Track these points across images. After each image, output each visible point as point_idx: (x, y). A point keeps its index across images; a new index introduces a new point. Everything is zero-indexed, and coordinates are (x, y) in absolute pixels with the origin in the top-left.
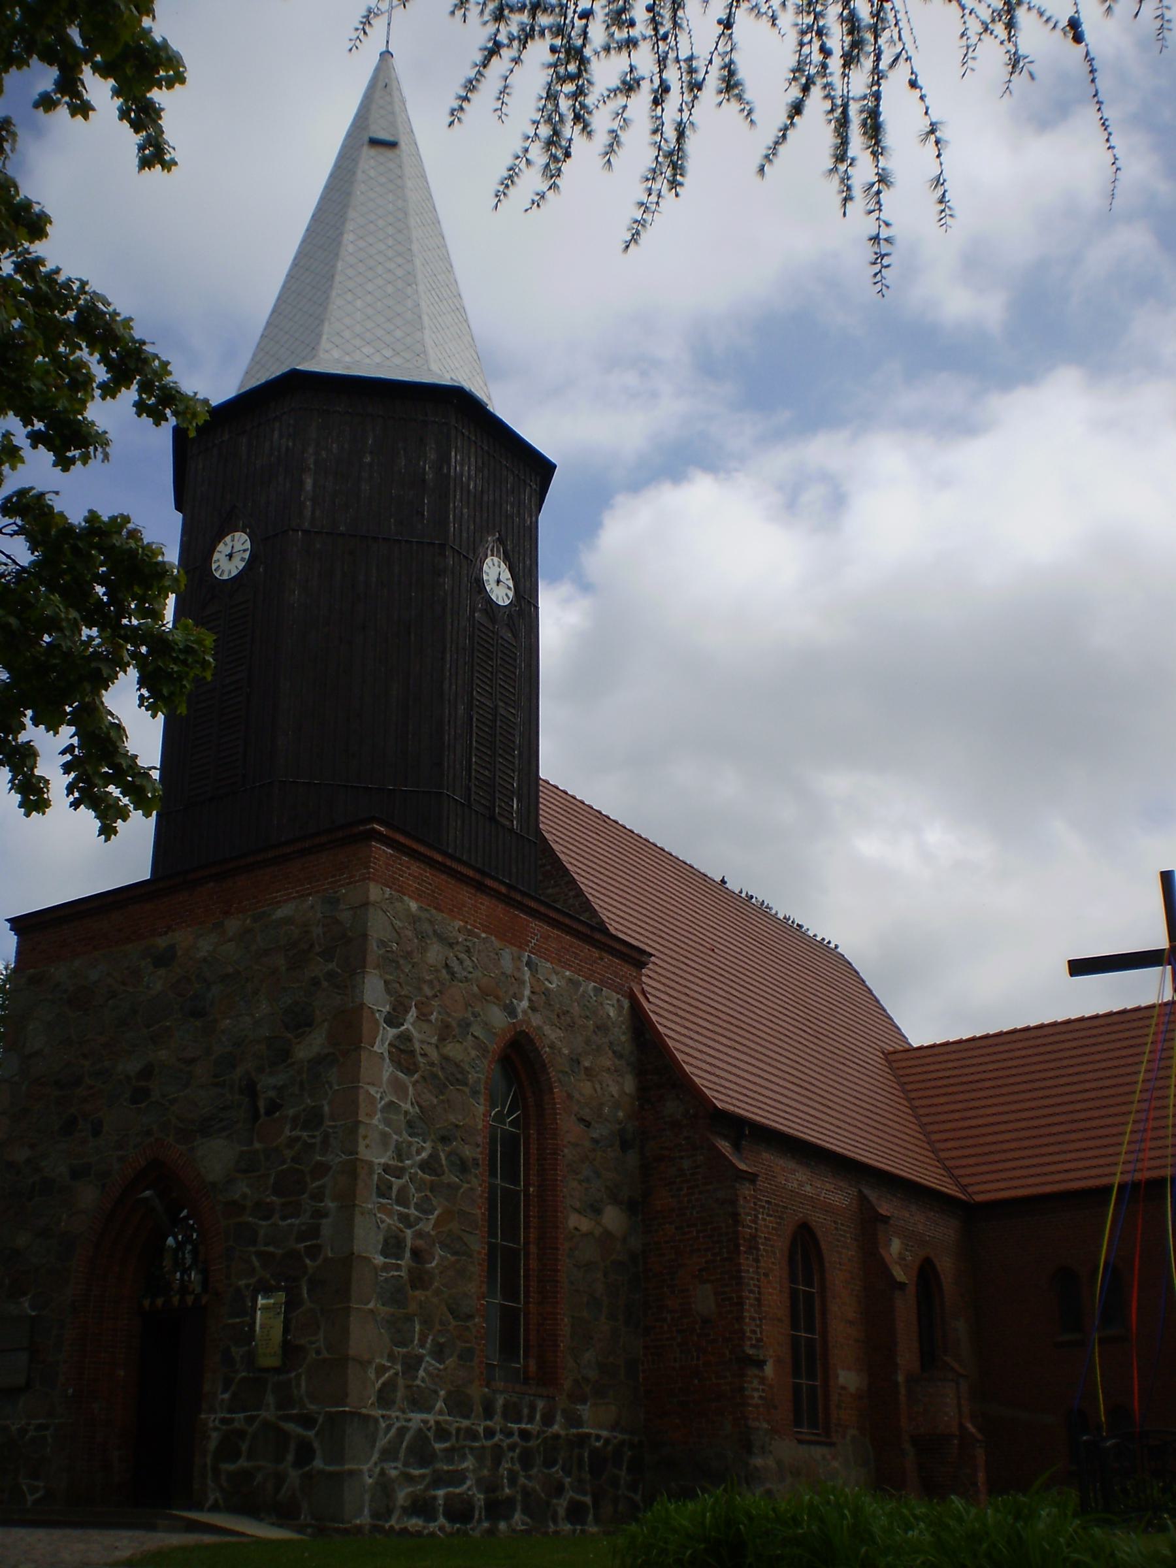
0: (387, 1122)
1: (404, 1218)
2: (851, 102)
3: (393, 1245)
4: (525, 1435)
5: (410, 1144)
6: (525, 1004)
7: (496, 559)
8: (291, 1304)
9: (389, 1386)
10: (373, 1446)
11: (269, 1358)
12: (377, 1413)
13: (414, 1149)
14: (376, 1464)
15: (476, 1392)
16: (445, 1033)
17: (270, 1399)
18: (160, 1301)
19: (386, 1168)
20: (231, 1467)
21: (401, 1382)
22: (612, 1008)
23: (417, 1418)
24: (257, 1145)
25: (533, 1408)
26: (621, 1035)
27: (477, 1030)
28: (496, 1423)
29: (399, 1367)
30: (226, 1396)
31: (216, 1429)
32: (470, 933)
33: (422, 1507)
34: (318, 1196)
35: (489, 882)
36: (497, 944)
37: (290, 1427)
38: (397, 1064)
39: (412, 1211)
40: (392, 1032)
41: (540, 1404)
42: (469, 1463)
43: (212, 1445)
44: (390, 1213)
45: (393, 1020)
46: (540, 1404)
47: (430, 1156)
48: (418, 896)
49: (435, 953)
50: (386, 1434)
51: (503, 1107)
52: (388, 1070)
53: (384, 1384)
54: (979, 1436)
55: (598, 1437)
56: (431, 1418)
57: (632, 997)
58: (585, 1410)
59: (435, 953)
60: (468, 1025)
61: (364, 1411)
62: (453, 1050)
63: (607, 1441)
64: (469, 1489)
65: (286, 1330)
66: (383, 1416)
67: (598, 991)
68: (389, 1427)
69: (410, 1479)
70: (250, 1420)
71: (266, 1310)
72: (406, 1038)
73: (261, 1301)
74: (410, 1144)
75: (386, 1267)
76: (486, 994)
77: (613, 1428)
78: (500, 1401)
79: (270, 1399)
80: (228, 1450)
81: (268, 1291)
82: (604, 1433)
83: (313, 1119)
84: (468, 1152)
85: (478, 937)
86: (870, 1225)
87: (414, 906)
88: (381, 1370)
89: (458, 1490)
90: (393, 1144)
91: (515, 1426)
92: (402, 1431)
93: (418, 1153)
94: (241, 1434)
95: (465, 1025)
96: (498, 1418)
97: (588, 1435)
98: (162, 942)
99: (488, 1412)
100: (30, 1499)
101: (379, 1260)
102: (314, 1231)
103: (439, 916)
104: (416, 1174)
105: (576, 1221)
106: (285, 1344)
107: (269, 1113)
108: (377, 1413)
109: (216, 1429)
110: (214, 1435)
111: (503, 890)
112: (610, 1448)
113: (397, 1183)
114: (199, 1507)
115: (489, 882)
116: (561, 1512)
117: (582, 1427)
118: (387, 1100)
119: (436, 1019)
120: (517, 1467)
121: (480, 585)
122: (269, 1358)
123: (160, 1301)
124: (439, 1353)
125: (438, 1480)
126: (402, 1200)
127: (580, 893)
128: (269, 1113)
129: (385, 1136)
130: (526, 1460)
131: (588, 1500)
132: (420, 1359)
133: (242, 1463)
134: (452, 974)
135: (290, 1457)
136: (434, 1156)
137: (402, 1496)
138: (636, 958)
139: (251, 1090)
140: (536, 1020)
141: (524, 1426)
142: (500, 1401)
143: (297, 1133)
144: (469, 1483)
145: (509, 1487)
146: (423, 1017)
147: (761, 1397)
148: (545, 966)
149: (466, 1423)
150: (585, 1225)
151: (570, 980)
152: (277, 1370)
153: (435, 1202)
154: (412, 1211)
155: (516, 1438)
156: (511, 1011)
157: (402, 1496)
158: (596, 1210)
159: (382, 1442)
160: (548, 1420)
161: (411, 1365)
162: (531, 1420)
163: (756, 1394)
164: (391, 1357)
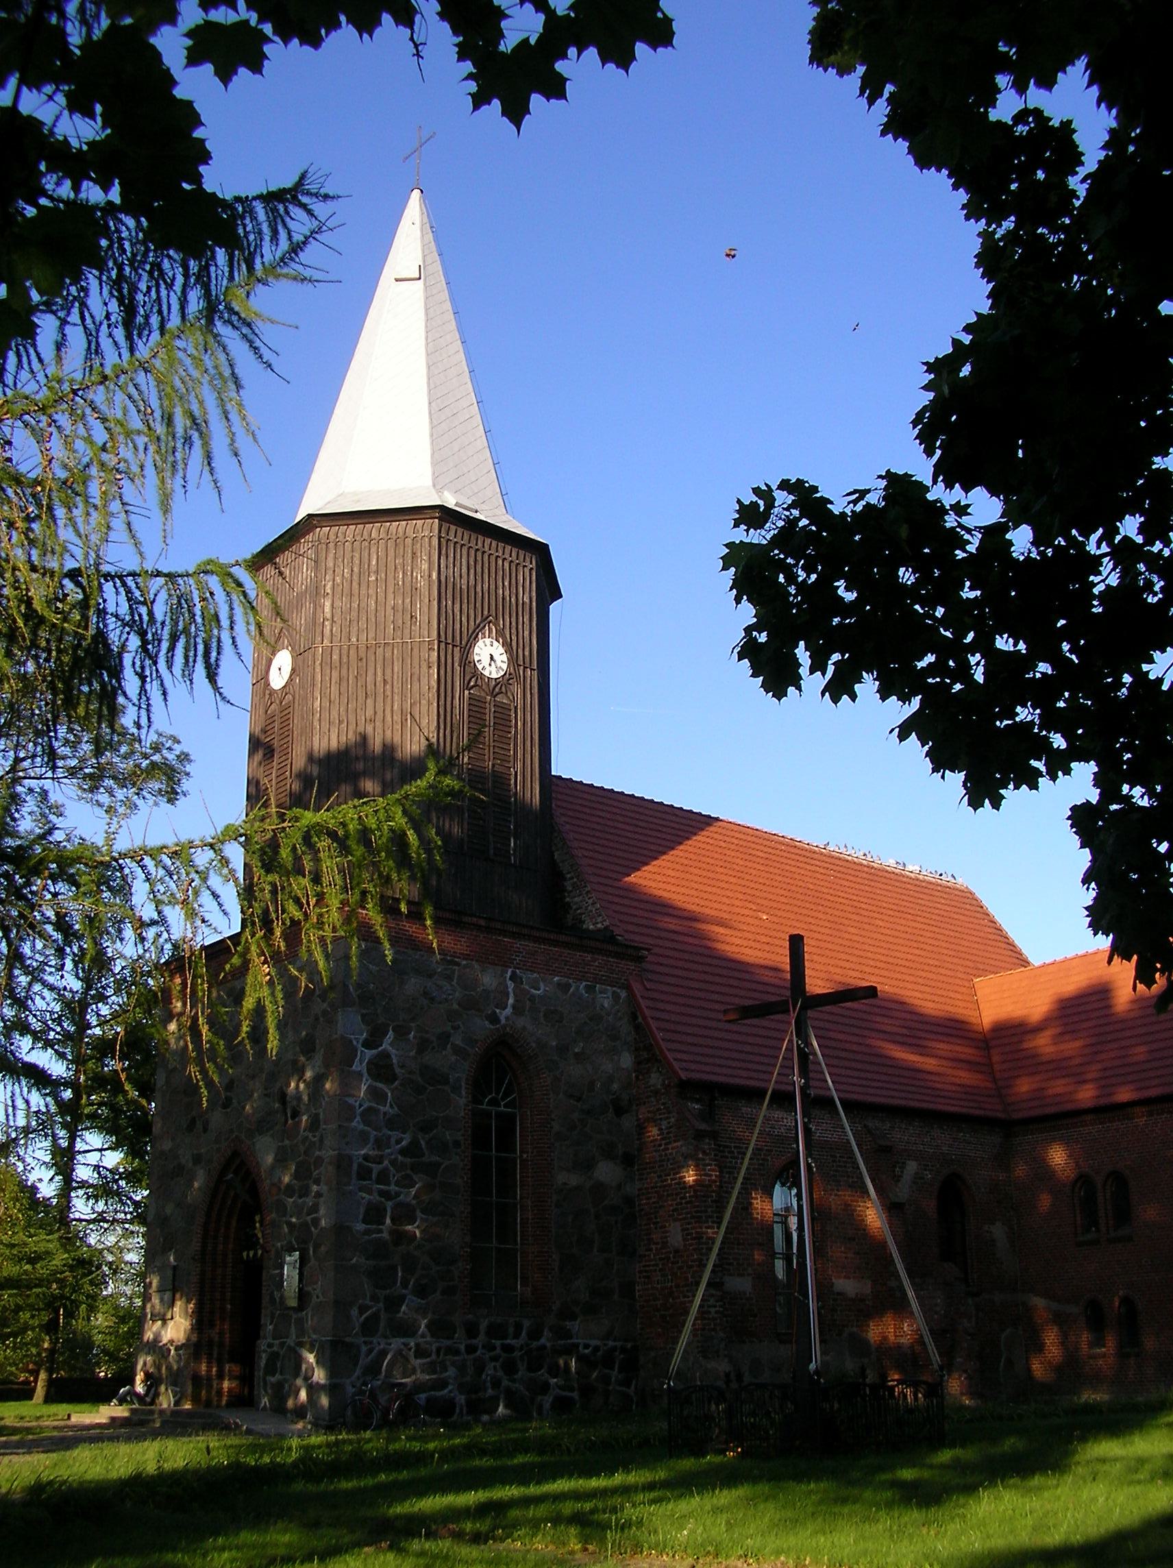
1: (386, 1195)
5: (390, 1137)
6: (509, 1011)
7: (488, 641)
10: (356, 1364)
13: (393, 1140)
14: (358, 1378)
19: (366, 1158)
21: (383, 1315)
24: (287, 1142)
25: (519, 1327)
27: (457, 1040)
29: (381, 1305)
31: (265, 1351)
35: (466, 919)
40: (370, 1053)
41: (527, 1323)
42: (451, 1372)
44: (370, 1192)
45: (368, 1044)
46: (527, 1323)
47: (411, 1143)
50: (367, 1356)
51: (497, 1093)
53: (367, 1319)
55: (586, 1346)
60: (448, 1036)
61: (348, 1339)
63: (596, 1349)
64: (450, 1392)
65: (300, 1280)
66: (365, 1343)
67: (589, 989)
68: (370, 1351)
70: (282, 1345)
72: (386, 1055)
74: (390, 1137)
75: (367, 1232)
78: (483, 1326)
85: (458, 964)
88: (362, 1309)
90: (372, 1140)
91: (498, 1343)
93: (398, 1142)
95: (444, 1038)
97: (577, 1346)
98: (428, 911)
101: (360, 1227)
104: (396, 1159)
106: (300, 1290)
109: (265, 1351)
110: (264, 1355)
111: (482, 922)
112: (600, 1353)
113: (376, 1168)
115: (466, 919)
116: (547, 1406)
117: (571, 1338)
118: (365, 1106)
119: (415, 1037)
120: (500, 1373)
126: (383, 1178)
129: (363, 1133)
131: (575, 1395)
136: (414, 1143)
140: (521, 1022)
141: (508, 1341)
142: (483, 1326)
144: (450, 1387)
145: (493, 1389)
146: (401, 1033)
147: (716, 1312)
150: (574, 1180)
151: (559, 984)
153: (415, 1178)
155: (498, 1351)
156: (494, 1019)
158: (587, 1166)
159: (364, 1361)
160: (535, 1334)
162: (516, 1336)
163: (713, 1310)
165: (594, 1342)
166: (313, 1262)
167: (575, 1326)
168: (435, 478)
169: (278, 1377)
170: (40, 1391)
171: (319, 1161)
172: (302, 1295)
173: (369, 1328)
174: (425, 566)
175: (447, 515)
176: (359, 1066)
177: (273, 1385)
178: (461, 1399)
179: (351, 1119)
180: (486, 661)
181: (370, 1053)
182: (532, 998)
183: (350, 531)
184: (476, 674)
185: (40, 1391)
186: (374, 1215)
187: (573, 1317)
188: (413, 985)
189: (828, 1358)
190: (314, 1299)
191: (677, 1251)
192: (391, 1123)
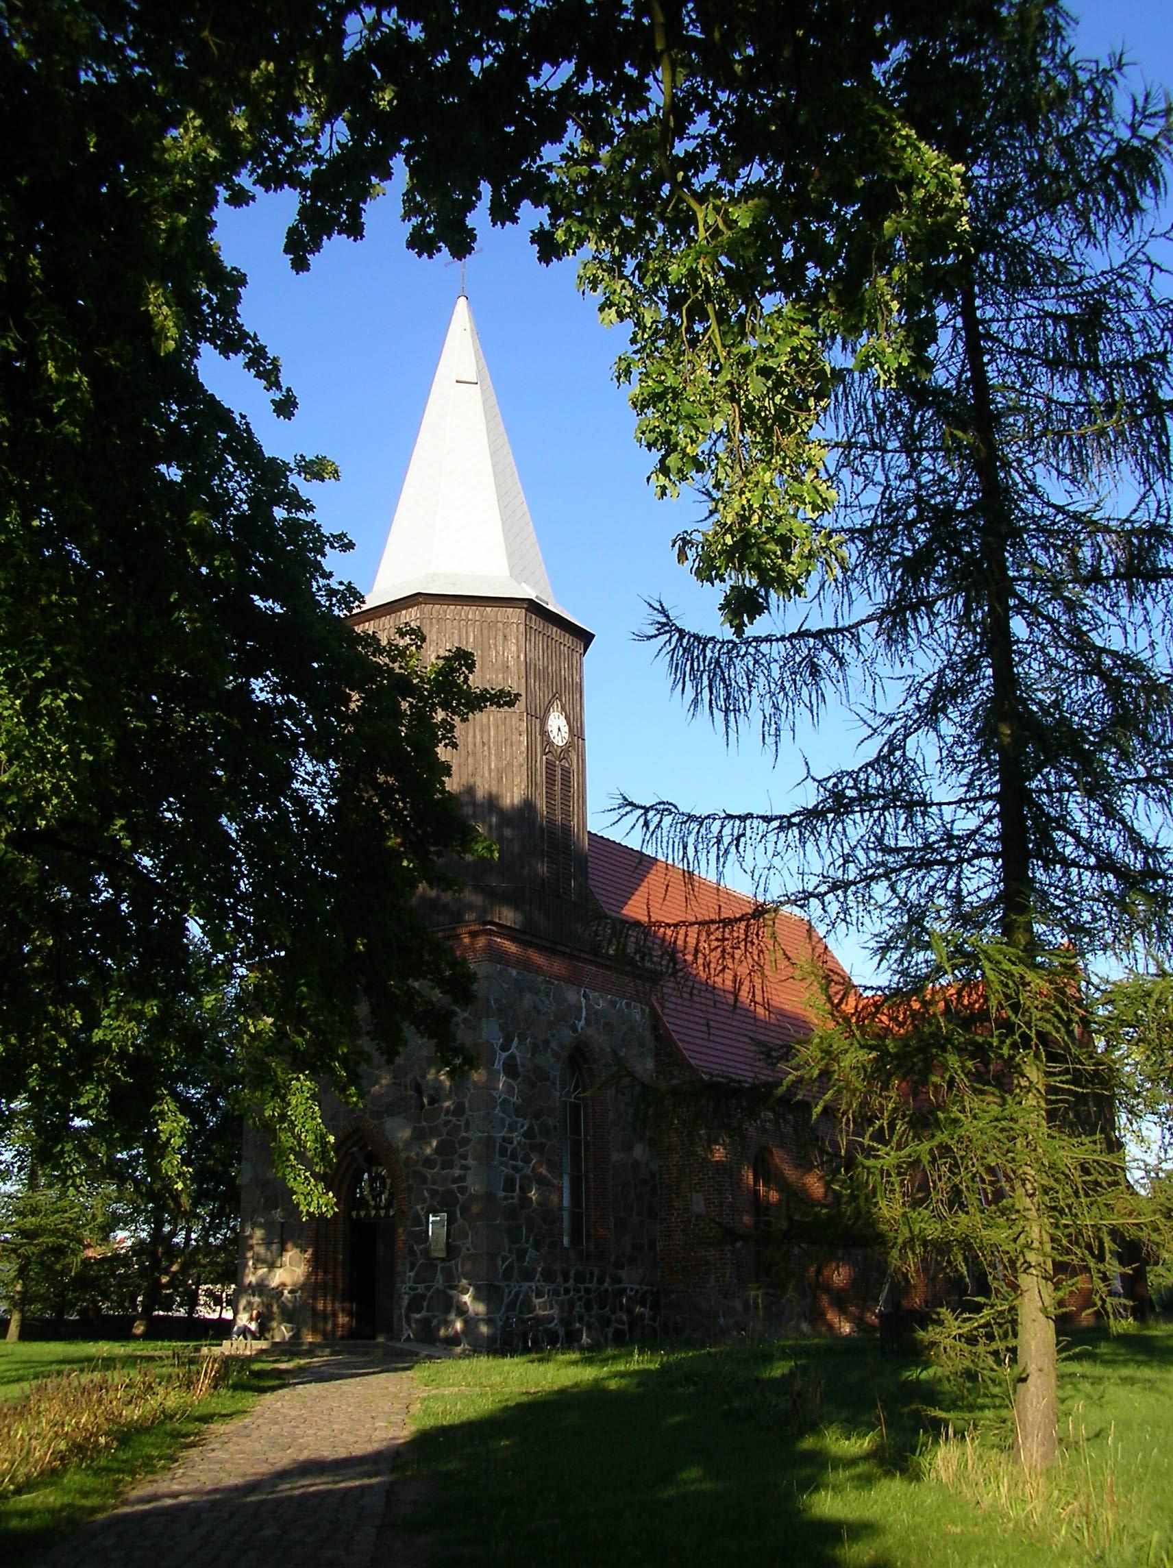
0: (504, 1111)
1: (515, 1168)
2: (723, 916)
4: (588, 1291)
6: (583, 1022)
8: (450, 1221)
9: (510, 1268)
11: (439, 1252)
12: (502, 1284)
16: (535, 1049)
17: (439, 1276)
18: (363, 1213)
20: (418, 1316)
25: (592, 1274)
27: (554, 1045)
34: (464, 1157)
38: (507, 1074)
39: (520, 1163)
40: (505, 1055)
43: (405, 1302)
45: (504, 1048)
46: (596, 1272)
58: (623, 1274)
67: (628, 1005)
70: (428, 1288)
72: (512, 1057)
73: (431, 1218)
75: (506, 1198)
77: (640, 1283)
78: (572, 1273)
79: (439, 1276)
80: (415, 1305)
84: (551, 1122)
88: (504, 1259)
89: (924, 1375)
92: (517, 1294)
94: (423, 1297)
95: (546, 1043)
96: (571, 1281)
99: (566, 1279)
105: (616, 1156)
106: (447, 1243)
122: (439, 1252)
123: (363, 1213)
124: (537, 1245)
126: (514, 1157)
129: (503, 1120)
130: (588, 1306)
132: (525, 1251)
134: (539, 1012)
136: (531, 1127)
140: (590, 1031)
142: (572, 1273)
146: (521, 1041)
148: (593, 995)
152: (443, 1260)
154: (520, 1163)
156: (575, 1029)
158: (628, 1148)
159: (507, 1300)
160: (601, 1281)
161: (521, 1254)
165: (636, 1287)
166: (460, 1221)
167: (623, 1274)
168: (511, 568)
169: (424, 1313)
170: (14, 1329)
171: (465, 1142)
172: (451, 1249)
173: (507, 1275)
174: (514, 648)
175: (534, 608)
176: (498, 1065)
177: (417, 1321)
178: (562, 1332)
179: (494, 1108)
180: (555, 731)
181: (505, 1055)
182: (596, 1012)
183: (451, 610)
184: (550, 743)
185: (14, 1329)
186: (509, 1185)
187: (622, 1267)
188: (528, 1000)
189: (1061, 1294)
190: (464, 1251)
191: (698, 1216)
192: (518, 1111)
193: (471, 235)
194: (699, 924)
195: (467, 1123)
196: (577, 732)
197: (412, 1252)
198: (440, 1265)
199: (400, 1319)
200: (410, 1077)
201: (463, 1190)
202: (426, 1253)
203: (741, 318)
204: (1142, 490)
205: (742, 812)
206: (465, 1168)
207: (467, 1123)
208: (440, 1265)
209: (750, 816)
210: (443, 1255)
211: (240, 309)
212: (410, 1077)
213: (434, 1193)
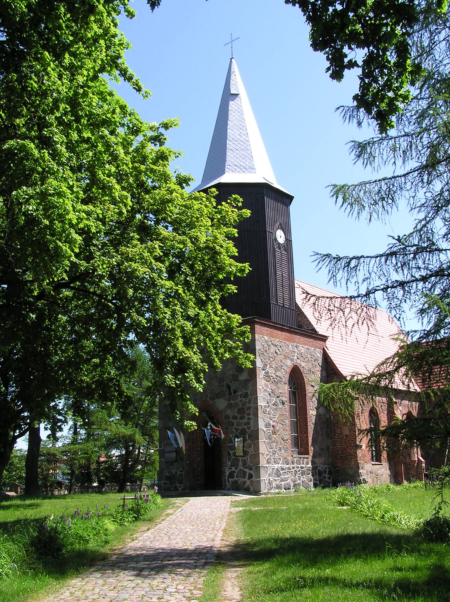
3: (267, 425)
8: (244, 441)
15: (290, 458)
16: (277, 370)
20: (232, 480)
22: (319, 355)
23: (276, 466)
26: (320, 361)
28: (295, 465)
30: (230, 463)
32: (281, 342)
33: (278, 487)
34: (249, 414)
36: (288, 343)
37: (246, 470)
48: (267, 335)
49: (273, 349)
52: (264, 382)
54: (423, 461)
56: (279, 465)
57: (324, 350)
59: (273, 349)
62: (278, 374)
65: (243, 447)
69: (275, 480)
71: (238, 442)
76: (286, 357)
77: (323, 464)
80: (231, 475)
81: (238, 437)
82: (321, 466)
83: (246, 395)
84: (284, 399)
86: (390, 405)
87: (266, 338)
100: (180, 489)
101: (265, 429)
102: (249, 423)
103: (272, 339)
106: (243, 450)
107: (234, 393)
108: (267, 465)
114: (225, 490)
121: (276, 239)
125: (282, 480)
127: (308, 320)
128: (234, 393)
133: (235, 479)
135: (247, 477)
137: (274, 485)
138: (324, 338)
139: (229, 387)
140: (299, 361)
143: (242, 399)
146: (271, 367)
149: (288, 466)
157: (274, 485)
164: (269, 452)
190: (250, 453)
193: (62, 429)
194: (341, 298)
195: (250, 400)
196: (288, 241)
197: (229, 454)
198: (241, 458)
199: (225, 481)
200: (225, 383)
201: (249, 428)
202: (234, 454)
203: (43, 75)
204: (116, 72)
205: (360, 255)
206: (249, 419)
207: (250, 400)
208: (241, 458)
209: (362, 257)
210: (242, 454)
211: (307, 28)
212: (225, 383)
213: (237, 430)
